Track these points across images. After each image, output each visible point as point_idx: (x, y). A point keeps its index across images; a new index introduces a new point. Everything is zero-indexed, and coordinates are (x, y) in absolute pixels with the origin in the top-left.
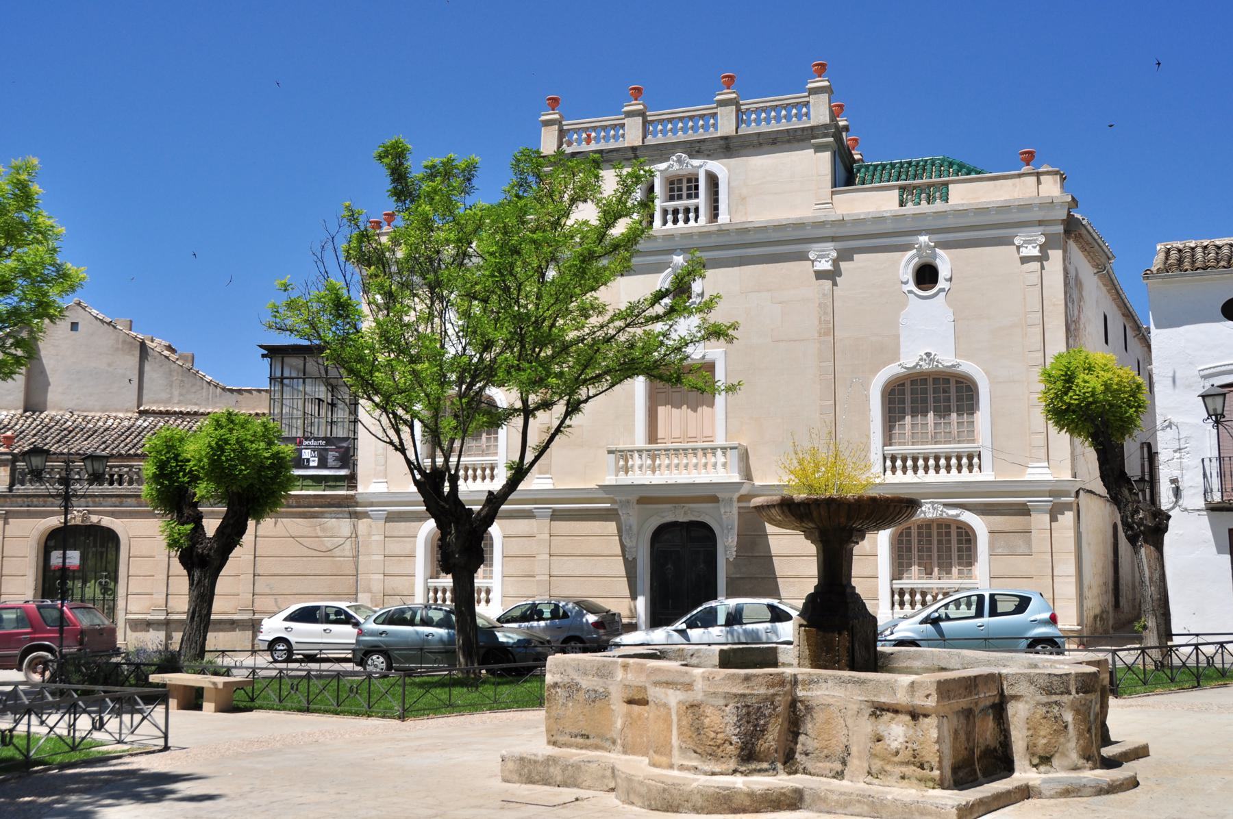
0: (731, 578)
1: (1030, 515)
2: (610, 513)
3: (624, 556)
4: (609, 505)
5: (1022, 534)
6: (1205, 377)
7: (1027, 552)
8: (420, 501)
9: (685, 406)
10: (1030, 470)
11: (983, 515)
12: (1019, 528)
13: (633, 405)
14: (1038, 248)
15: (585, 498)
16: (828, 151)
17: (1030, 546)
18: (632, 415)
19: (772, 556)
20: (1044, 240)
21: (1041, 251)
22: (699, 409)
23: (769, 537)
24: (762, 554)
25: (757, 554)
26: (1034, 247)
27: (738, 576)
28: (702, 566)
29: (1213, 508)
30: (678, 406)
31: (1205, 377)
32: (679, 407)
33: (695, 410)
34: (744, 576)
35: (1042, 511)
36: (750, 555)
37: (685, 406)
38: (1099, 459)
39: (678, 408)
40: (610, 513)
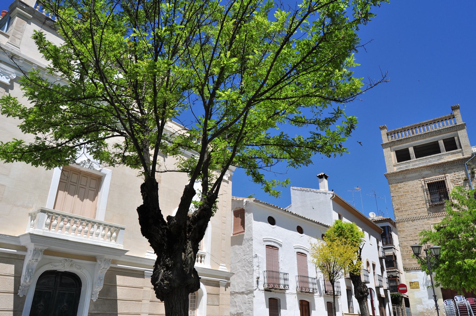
0: (90, 313)
1: (219, 287)
2: (12, 257)
3: (16, 293)
4: (16, 251)
5: (216, 295)
6: (265, 241)
7: (218, 304)
8: (151, 266)
9: (77, 196)
10: (220, 267)
11: (206, 285)
12: (215, 293)
13: (49, 184)
14: (9, 79)
15: (9, 244)
16: (15, 17)
17: (219, 302)
18: (47, 190)
19: (116, 300)
20: (15, 77)
21: (10, 82)
22: (85, 200)
23: (117, 287)
24: (112, 298)
25: (109, 298)
26: (7, 79)
27: (96, 312)
28: (65, 304)
29: (266, 290)
30: (72, 194)
31: (265, 241)
32: (73, 195)
33: (82, 200)
34: (99, 312)
35: (223, 286)
36: (105, 298)
37: (77, 196)
38: (153, 248)
39: (72, 195)
40: (12, 257)
